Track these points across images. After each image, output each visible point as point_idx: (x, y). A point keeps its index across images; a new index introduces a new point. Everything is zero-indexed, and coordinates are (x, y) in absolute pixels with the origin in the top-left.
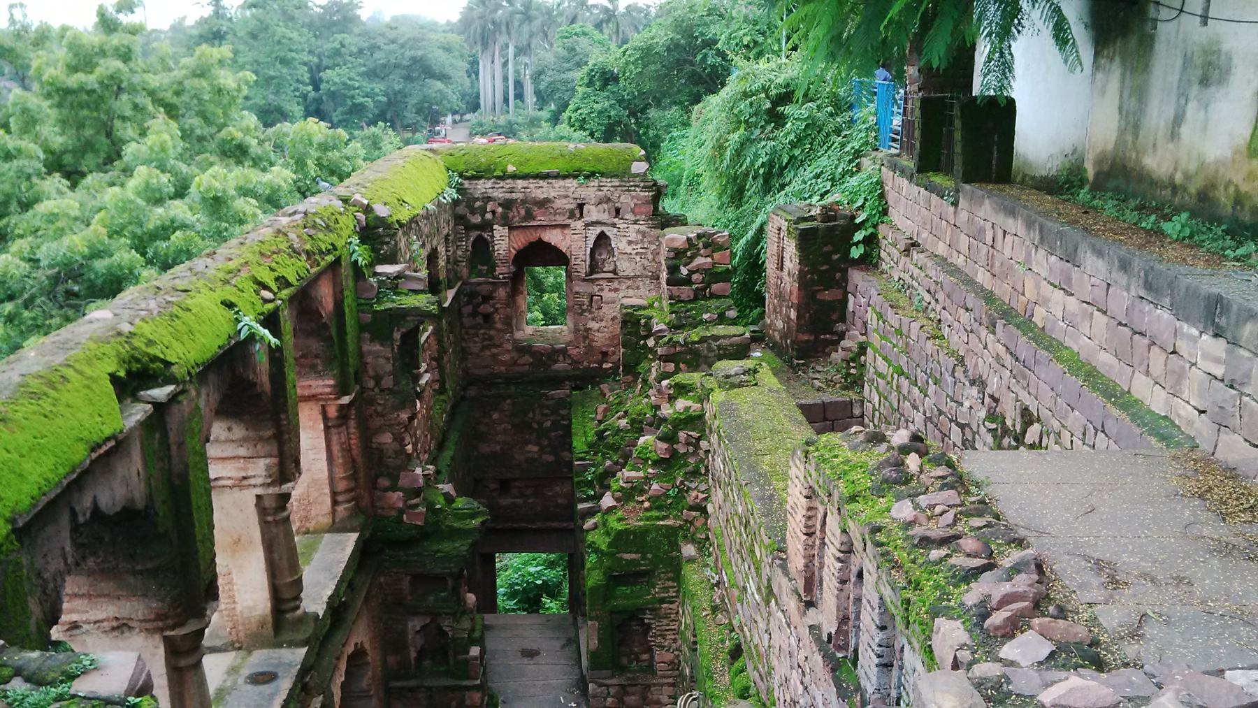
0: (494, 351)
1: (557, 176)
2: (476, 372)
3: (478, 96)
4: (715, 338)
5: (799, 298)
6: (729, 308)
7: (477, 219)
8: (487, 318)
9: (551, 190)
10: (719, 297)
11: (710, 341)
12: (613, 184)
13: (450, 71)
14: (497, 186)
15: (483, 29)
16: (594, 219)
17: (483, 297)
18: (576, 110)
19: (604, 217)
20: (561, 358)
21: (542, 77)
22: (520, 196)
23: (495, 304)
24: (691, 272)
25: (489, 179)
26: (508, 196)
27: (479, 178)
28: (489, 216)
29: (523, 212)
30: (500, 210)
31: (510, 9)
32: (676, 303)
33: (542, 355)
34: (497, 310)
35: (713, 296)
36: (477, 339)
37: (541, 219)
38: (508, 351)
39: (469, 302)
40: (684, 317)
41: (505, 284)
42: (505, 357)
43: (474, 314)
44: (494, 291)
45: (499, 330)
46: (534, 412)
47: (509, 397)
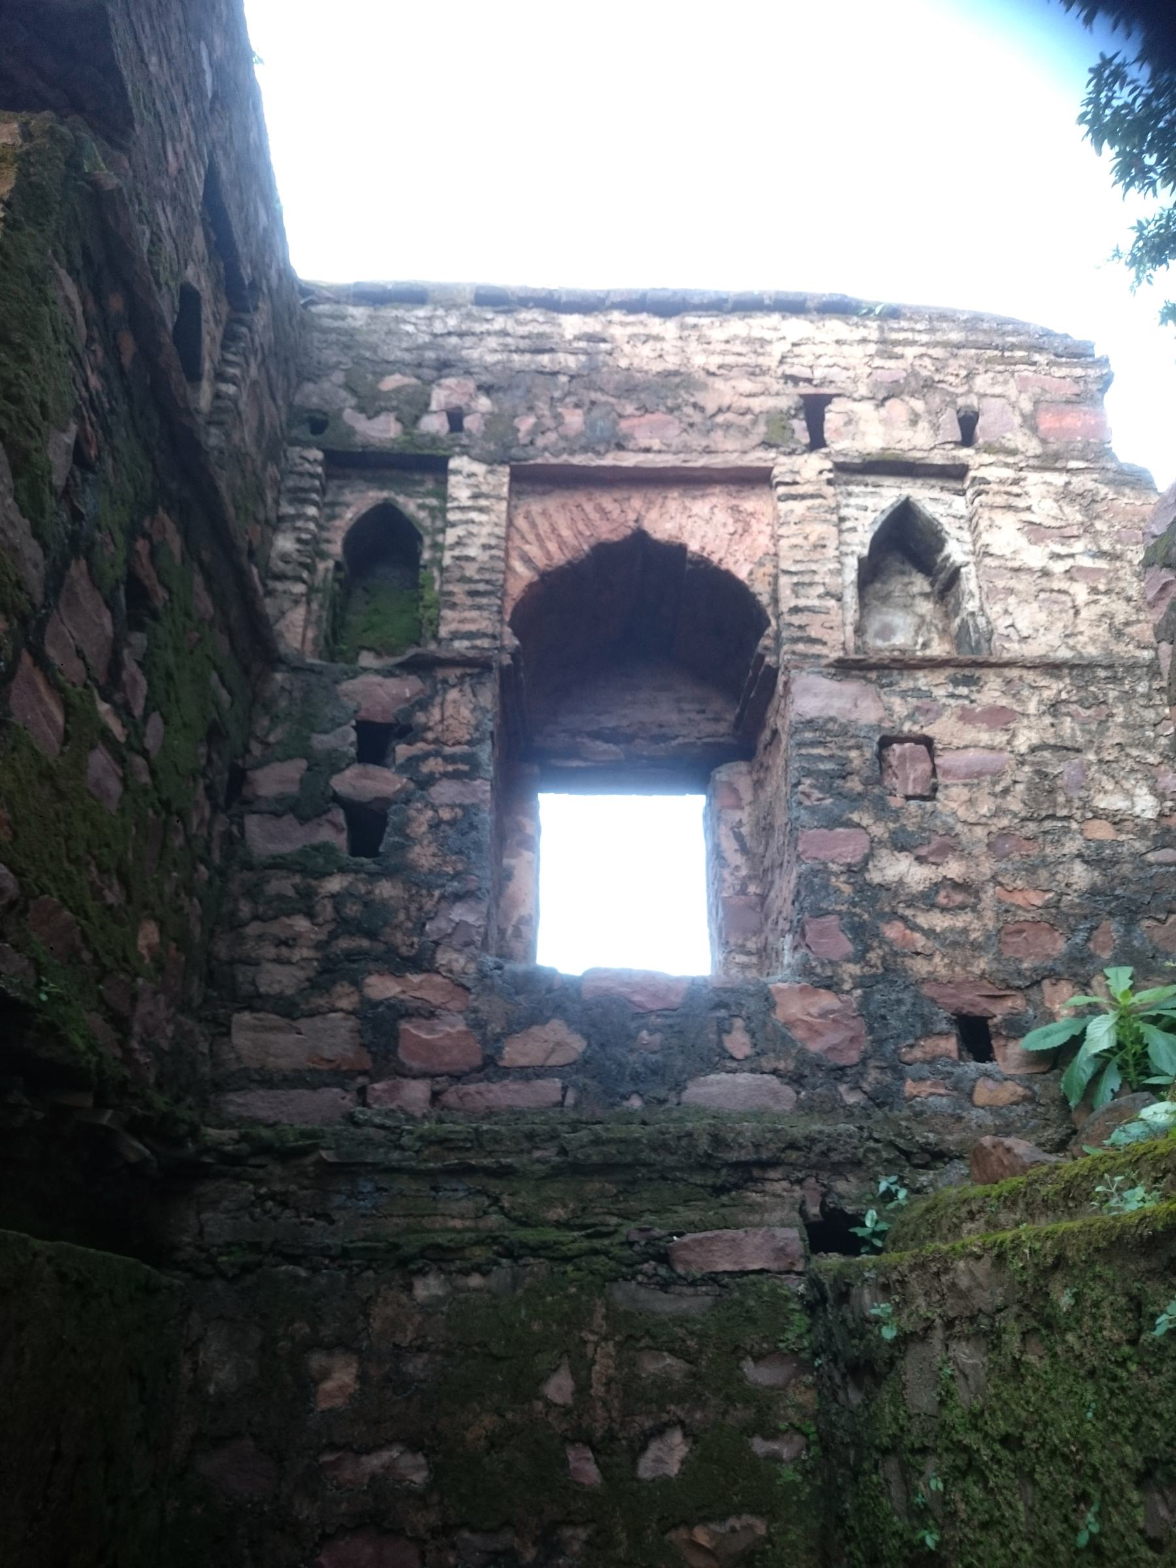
23: (414, 762)
36: (301, 924)
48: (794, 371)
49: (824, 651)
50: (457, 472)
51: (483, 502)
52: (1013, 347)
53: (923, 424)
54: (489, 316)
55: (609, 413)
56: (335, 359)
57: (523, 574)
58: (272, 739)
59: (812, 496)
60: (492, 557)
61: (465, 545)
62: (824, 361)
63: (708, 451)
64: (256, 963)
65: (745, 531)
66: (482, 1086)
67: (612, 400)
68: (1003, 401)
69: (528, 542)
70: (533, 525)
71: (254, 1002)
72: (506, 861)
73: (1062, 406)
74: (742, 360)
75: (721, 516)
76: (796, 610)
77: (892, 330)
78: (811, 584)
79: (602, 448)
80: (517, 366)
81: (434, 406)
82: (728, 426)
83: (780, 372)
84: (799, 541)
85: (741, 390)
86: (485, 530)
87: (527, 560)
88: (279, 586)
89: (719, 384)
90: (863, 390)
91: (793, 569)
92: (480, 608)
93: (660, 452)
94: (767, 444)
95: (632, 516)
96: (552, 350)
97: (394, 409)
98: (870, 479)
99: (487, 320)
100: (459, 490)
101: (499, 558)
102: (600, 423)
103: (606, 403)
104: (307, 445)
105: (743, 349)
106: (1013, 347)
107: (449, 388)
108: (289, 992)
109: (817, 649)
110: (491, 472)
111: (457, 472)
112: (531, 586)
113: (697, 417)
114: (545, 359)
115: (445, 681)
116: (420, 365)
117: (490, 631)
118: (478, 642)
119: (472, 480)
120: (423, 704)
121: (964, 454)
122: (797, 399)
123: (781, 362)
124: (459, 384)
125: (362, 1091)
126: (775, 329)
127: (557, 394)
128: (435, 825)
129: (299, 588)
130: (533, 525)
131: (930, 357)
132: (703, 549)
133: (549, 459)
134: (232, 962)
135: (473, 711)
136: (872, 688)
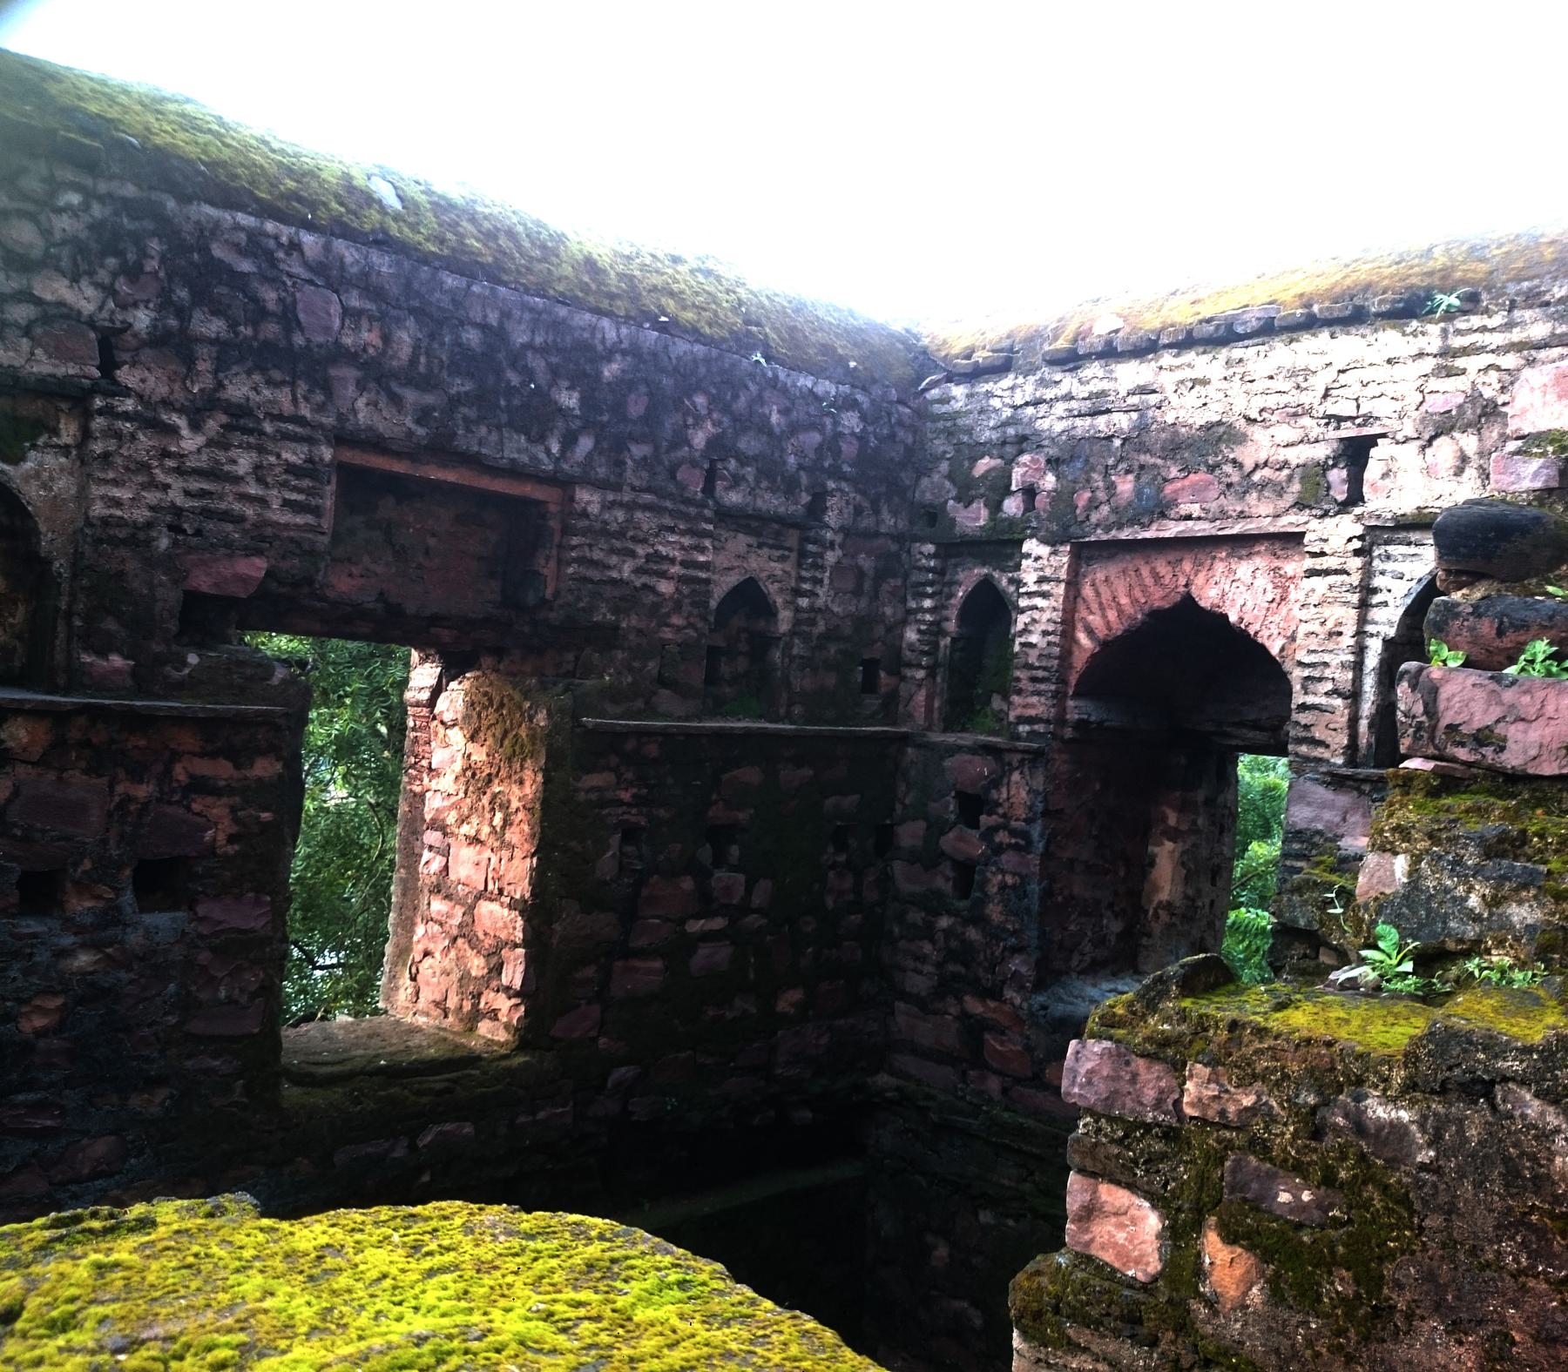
0: (974, 1006)
1: (1269, 329)
7: (974, 518)
23: (994, 829)
28: (1012, 506)
36: (927, 948)
41: (1035, 758)
49: (1326, 755)
50: (1028, 556)
51: (1045, 587)
53: (1471, 472)
54: (1057, 377)
55: (1154, 479)
56: (942, 448)
58: (907, 801)
59: (1337, 572)
60: (1049, 644)
61: (1030, 632)
62: (1373, 390)
63: (1242, 516)
64: (904, 970)
65: (1283, 599)
66: (1032, 1091)
67: (1159, 462)
69: (1092, 613)
70: (1098, 594)
71: (905, 996)
72: (1150, 848)
74: (1283, 399)
75: (1263, 581)
76: (1304, 707)
77: (1459, 332)
78: (1320, 679)
80: (1079, 432)
81: (1014, 488)
82: (1263, 486)
83: (1321, 410)
84: (1315, 627)
85: (1278, 440)
86: (1046, 616)
87: (1090, 632)
89: (1256, 432)
91: (1306, 660)
92: (1039, 693)
93: (1199, 518)
94: (1300, 505)
95: (1182, 581)
96: (1108, 411)
97: (982, 496)
99: (1057, 383)
101: (1055, 644)
102: (1147, 491)
103: (1155, 466)
104: (923, 540)
105: (1287, 385)
107: (1025, 465)
108: (923, 994)
109: (1319, 752)
110: (1054, 553)
111: (1028, 556)
112: (1093, 656)
113: (1235, 478)
114: (1101, 421)
115: (1010, 764)
116: (1004, 443)
117: (1045, 716)
118: (1036, 727)
119: (1038, 565)
120: (996, 783)
123: (1326, 396)
124: (1033, 461)
125: (964, 1073)
128: (1003, 887)
129: (921, 674)
130: (1098, 594)
131: (1498, 369)
132: (1241, 619)
133: (1101, 535)
135: (1028, 792)
136: (1366, 801)
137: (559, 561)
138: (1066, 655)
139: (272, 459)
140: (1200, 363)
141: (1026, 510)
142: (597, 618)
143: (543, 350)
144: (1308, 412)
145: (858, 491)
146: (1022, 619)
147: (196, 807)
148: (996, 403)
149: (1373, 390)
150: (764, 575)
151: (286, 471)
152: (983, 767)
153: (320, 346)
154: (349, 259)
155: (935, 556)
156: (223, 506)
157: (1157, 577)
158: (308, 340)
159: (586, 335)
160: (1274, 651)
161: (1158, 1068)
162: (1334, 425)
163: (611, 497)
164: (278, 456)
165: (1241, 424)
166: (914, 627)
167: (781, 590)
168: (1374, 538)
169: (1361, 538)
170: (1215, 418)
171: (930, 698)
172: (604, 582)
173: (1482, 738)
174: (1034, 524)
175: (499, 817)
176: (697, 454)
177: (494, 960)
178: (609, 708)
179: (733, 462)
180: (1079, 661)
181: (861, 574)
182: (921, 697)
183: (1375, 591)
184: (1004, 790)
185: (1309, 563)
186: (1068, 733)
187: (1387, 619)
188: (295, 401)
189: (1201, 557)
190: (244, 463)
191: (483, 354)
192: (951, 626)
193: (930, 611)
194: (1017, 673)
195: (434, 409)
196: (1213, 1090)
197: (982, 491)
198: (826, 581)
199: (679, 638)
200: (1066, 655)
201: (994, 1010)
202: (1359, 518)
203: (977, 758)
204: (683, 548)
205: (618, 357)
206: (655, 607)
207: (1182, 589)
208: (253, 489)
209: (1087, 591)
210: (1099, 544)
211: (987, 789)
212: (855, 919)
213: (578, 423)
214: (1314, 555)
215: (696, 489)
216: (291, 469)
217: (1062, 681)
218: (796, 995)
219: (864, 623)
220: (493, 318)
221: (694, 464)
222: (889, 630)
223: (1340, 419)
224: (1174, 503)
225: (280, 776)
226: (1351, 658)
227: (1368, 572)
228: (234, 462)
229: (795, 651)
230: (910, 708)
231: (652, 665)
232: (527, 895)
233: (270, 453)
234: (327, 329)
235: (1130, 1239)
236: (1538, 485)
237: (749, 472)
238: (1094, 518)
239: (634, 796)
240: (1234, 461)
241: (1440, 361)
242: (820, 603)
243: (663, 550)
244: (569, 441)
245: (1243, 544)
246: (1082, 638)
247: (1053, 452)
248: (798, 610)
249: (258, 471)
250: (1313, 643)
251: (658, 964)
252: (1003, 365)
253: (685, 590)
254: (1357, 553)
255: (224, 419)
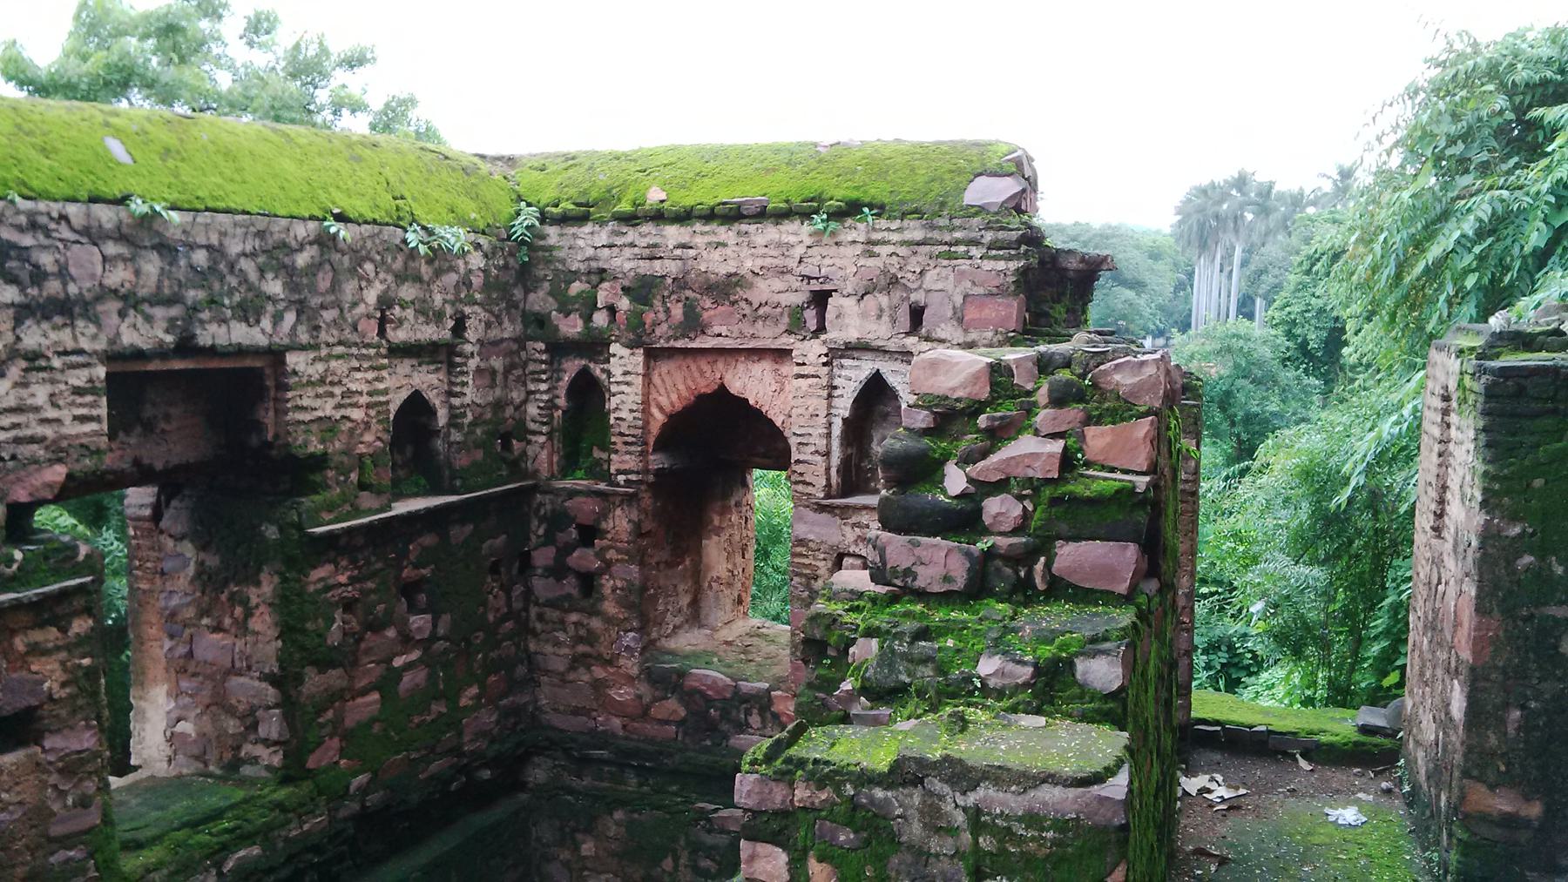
0: (599, 672)
1: (762, 215)
2: (558, 721)
3: (1190, 316)
4: (961, 775)
5: (1477, 644)
6: (1094, 645)
7: (571, 327)
8: (588, 582)
9: (745, 252)
10: (1083, 596)
11: (937, 785)
12: (908, 236)
13: (1147, 277)
14: (619, 241)
15: (1201, 226)
16: (852, 335)
17: (580, 528)
18: (1282, 309)
19: (880, 332)
20: (755, 720)
21: (1263, 277)
22: (671, 268)
23: (604, 549)
24: (983, 489)
25: (602, 223)
26: (645, 267)
27: (582, 219)
28: (600, 319)
29: (678, 311)
30: (624, 304)
31: (1241, 199)
32: (893, 599)
33: (709, 701)
34: (608, 564)
35: (1058, 589)
36: (561, 636)
37: (723, 330)
38: (630, 680)
39: (549, 539)
40: (907, 657)
41: (630, 499)
42: (622, 694)
43: (558, 571)
44: (604, 515)
45: (609, 620)
46: (676, 860)
47: (622, 803)
48: (806, 272)
51: (628, 378)
52: (957, 243)
53: (885, 318)
57: (659, 417)
59: (813, 376)
63: (753, 336)
67: (699, 296)
68: (943, 294)
70: (663, 381)
73: (985, 299)
75: (769, 377)
76: (798, 462)
78: (807, 444)
79: (692, 335)
81: (599, 305)
86: (632, 398)
87: (661, 409)
88: (534, 438)
90: (850, 290)
92: (630, 453)
94: (789, 332)
96: (661, 258)
98: (856, 355)
100: (616, 367)
104: (535, 339)
106: (957, 243)
109: (809, 489)
112: (664, 425)
113: (747, 311)
118: (630, 477)
121: (911, 342)
122: (808, 294)
124: (611, 287)
126: (795, 234)
127: (666, 294)
129: (542, 439)
133: (662, 343)
134: (536, 653)
137: (276, 411)
138: (645, 427)
139: (63, 387)
140: (724, 233)
141: (610, 322)
142: (311, 449)
143: (253, 255)
144: (790, 272)
145: (486, 311)
146: (614, 401)
147: (34, 668)
148: (581, 243)
149: (827, 261)
150: (425, 386)
151: (73, 393)
152: (592, 506)
153: (89, 290)
154: (104, 219)
155: (546, 351)
156: (28, 432)
157: (702, 373)
158: (80, 288)
159: (283, 236)
160: (778, 424)
161: (782, 785)
162: (806, 281)
163: (312, 356)
164: (66, 383)
165: (749, 276)
166: (536, 404)
167: (438, 395)
168: (835, 355)
169: (826, 355)
170: (733, 270)
171: (550, 456)
172: (311, 421)
173: (908, 572)
174: (617, 333)
175: (238, 611)
176: (371, 308)
177: (249, 721)
178: (327, 517)
179: (397, 307)
180: (655, 428)
181: (493, 372)
182: (544, 455)
183: (835, 388)
184: (611, 521)
185: (797, 370)
186: (651, 478)
187: (844, 406)
188: (75, 338)
189: (729, 359)
190: (40, 395)
191: (209, 268)
192: (562, 402)
193: (546, 392)
194: (613, 439)
195: (177, 319)
196: (808, 793)
197: (577, 306)
198: (471, 382)
199: (371, 450)
200: (645, 427)
201: (613, 674)
202: (824, 342)
203: (589, 500)
204: (368, 382)
205: (308, 247)
206: (352, 431)
207: (719, 381)
208: (51, 413)
209: (656, 379)
210: (662, 349)
211: (598, 521)
212: (509, 625)
213: (283, 304)
214: (798, 364)
215: (373, 336)
216: (78, 391)
217: (645, 443)
218: (474, 690)
219: (498, 405)
220: (214, 240)
221: (369, 316)
222: (517, 408)
223: (810, 278)
224: (709, 325)
225: (92, 629)
226: (825, 431)
227: (831, 376)
228: (33, 395)
229: (452, 438)
230: (536, 465)
231: (354, 476)
232: (276, 670)
233: (59, 382)
234: (93, 276)
235: (774, 866)
236: (924, 426)
237: (410, 313)
238: (658, 332)
239: (349, 578)
240: (746, 300)
241: (866, 247)
242: (467, 400)
243: (353, 387)
244: (277, 318)
245: (758, 354)
246: (655, 411)
247: (626, 283)
248: (452, 407)
249: (53, 400)
250: (802, 421)
251: (375, 696)
252: (579, 217)
253: (372, 413)
254: (824, 364)
255: (24, 364)
